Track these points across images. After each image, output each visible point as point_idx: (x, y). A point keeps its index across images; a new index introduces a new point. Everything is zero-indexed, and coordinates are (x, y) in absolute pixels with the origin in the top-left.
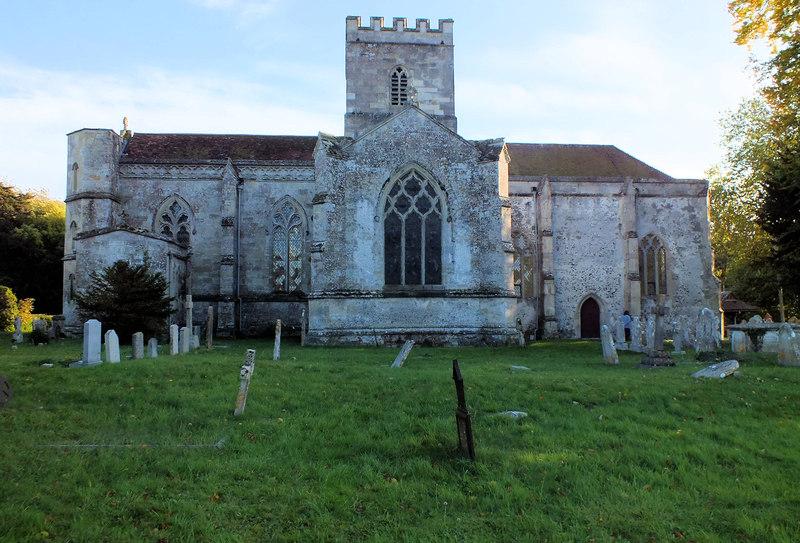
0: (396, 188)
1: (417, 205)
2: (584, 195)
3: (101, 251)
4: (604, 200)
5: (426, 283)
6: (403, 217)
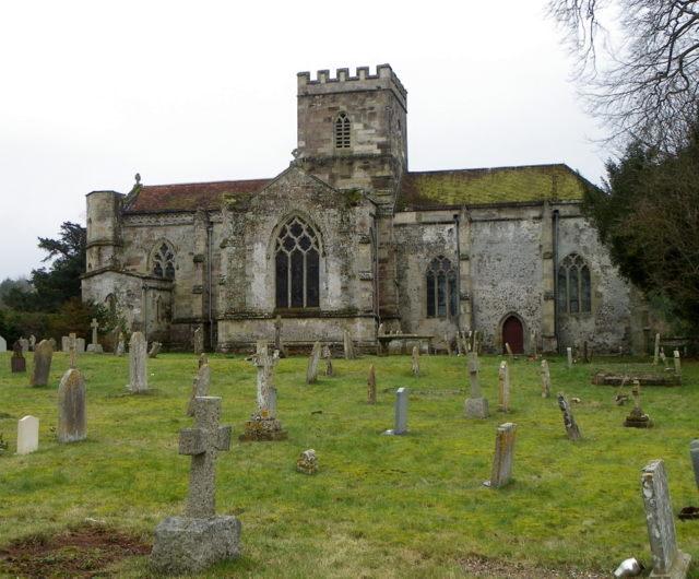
0: (283, 232)
1: (300, 244)
2: (503, 220)
3: (98, 286)
4: (524, 224)
5: (308, 306)
6: (289, 254)
